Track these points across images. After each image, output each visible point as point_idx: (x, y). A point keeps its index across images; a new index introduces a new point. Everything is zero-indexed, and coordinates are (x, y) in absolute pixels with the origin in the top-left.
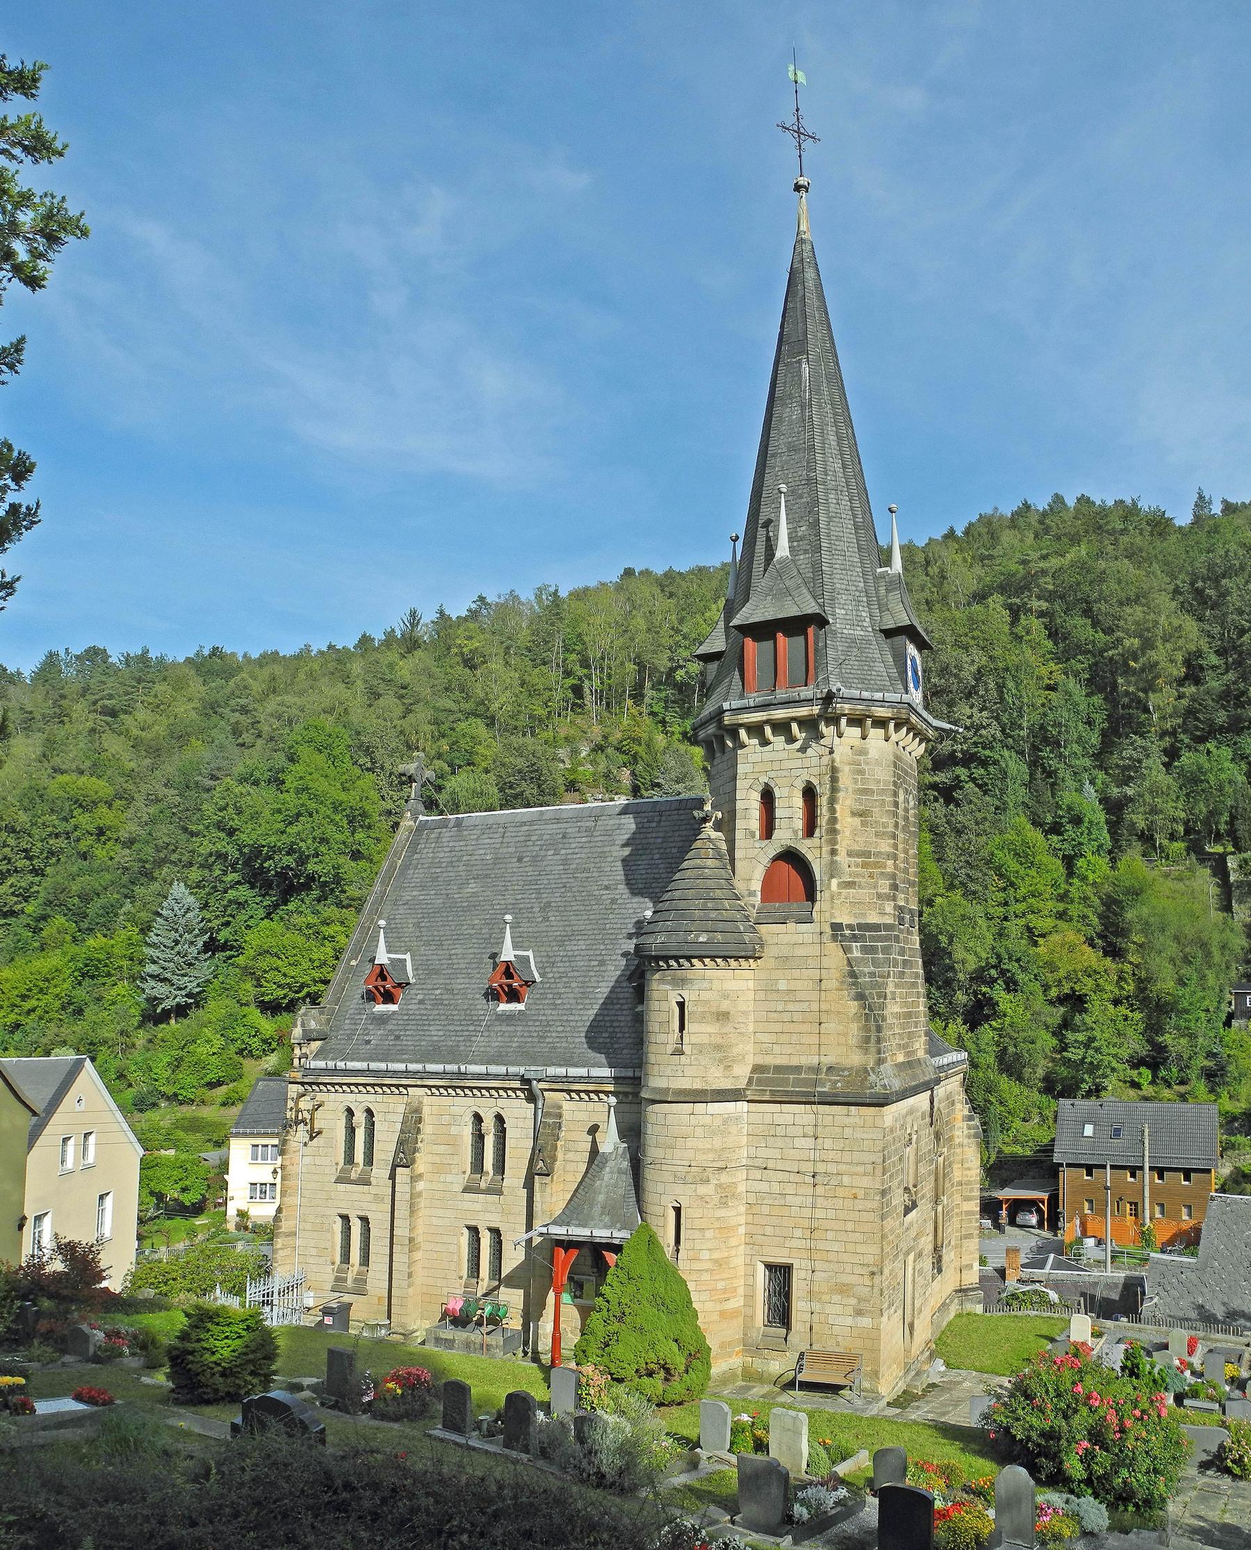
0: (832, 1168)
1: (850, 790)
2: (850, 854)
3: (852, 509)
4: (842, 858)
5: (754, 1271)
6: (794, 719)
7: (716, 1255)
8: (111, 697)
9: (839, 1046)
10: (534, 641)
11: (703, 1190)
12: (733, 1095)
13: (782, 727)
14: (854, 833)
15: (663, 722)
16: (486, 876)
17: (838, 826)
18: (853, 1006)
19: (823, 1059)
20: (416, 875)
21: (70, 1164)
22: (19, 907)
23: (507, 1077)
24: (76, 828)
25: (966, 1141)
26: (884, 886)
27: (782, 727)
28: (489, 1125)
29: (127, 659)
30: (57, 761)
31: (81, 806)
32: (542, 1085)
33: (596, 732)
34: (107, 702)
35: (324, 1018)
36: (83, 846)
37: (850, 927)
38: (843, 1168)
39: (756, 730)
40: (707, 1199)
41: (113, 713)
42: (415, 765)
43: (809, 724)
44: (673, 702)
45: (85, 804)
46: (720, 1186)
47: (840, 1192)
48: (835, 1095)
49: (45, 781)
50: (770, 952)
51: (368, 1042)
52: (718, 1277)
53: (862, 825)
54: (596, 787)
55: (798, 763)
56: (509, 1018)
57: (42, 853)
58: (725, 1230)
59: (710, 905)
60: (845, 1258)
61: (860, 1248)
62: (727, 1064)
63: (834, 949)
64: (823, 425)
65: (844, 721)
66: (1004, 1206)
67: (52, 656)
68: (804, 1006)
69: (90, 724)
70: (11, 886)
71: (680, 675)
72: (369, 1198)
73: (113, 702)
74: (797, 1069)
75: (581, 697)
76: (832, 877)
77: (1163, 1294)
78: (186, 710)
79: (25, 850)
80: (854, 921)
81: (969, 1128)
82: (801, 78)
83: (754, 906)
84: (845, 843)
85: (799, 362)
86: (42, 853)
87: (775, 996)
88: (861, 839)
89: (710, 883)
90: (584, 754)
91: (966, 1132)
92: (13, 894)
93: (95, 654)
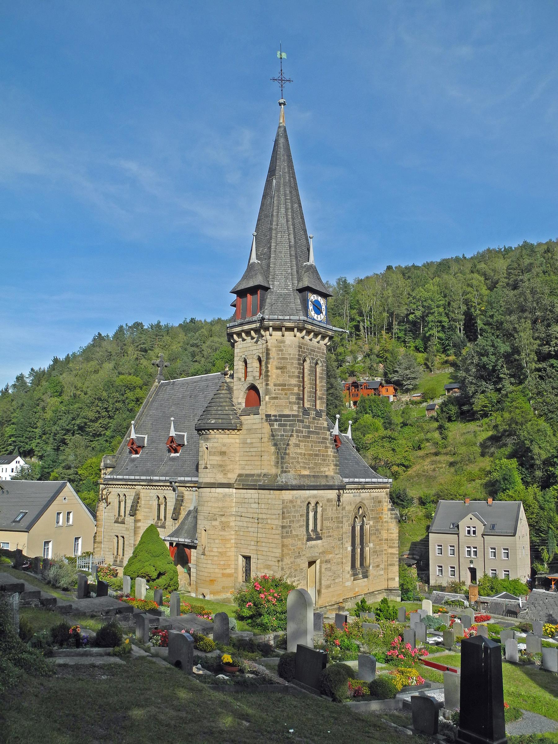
0: (264, 516)
1: (276, 358)
2: (275, 385)
3: (289, 239)
4: (271, 387)
5: (238, 558)
6: (252, 329)
7: (220, 550)
8: (144, 343)
9: (267, 466)
10: (335, 305)
11: (214, 523)
12: (228, 486)
13: (248, 333)
14: (278, 376)
15: (404, 342)
16: (178, 404)
17: (269, 374)
18: (273, 449)
19: (262, 471)
20: (155, 404)
21: (61, 523)
22: (104, 432)
23: (165, 481)
24: (127, 398)
25: (389, 520)
26: (293, 399)
27: (248, 333)
28: (162, 500)
29: (152, 326)
30: (120, 369)
31: (129, 389)
32: (177, 484)
33: (366, 348)
34: (142, 346)
35: (114, 460)
36: (130, 406)
37: (274, 416)
38: (268, 516)
39: (239, 334)
40: (216, 527)
41: (146, 351)
42: (158, 361)
43: (257, 331)
44: (409, 331)
45: (132, 388)
46: (222, 522)
47: (267, 526)
48: (264, 486)
49: (115, 378)
50: (244, 427)
51: (127, 469)
52: (221, 559)
53: (282, 373)
54: (365, 374)
55: (255, 348)
56: (173, 459)
57: (113, 409)
58: (225, 540)
59: (219, 408)
60: (269, 554)
61: (275, 550)
62: (225, 473)
63: (266, 425)
64: (279, 204)
65: (271, 329)
66: (553, 583)
67: (121, 327)
68: (255, 449)
69: (135, 356)
70: (100, 423)
71: (411, 317)
72: (124, 529)
73: (145, 346)
74: (253, 475)
75: (359, 331)
76: (266, 395)
77: (533, 608)
78: (176, 347)
79: (106, 408)
80: (277, 413)
81: (391, 514)
82: (284, 55)
83: (240, 409)
84: (273, 381)
85: (272, 179)
86: (113, 409)
87: (246, 445)
88: (281, 379)
89: (222, 400)
90: (360, 359)
91: (390, 516)
92: (101, 427)
93: (138, 325)
